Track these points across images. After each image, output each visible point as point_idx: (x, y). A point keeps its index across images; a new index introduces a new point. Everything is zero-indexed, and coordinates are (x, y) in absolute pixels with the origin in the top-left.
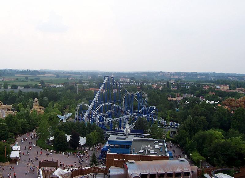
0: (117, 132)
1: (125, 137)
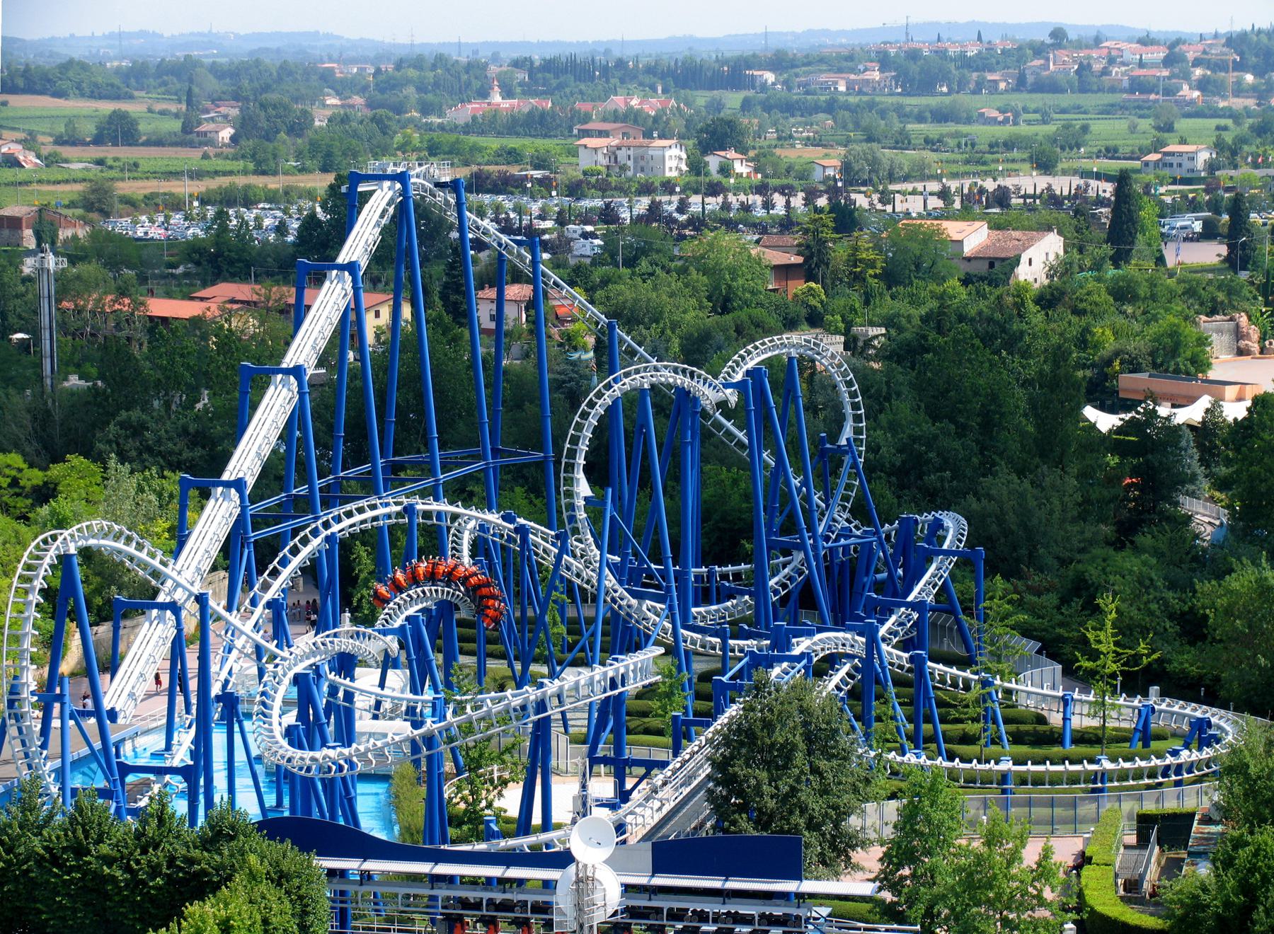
0: (495, 871)
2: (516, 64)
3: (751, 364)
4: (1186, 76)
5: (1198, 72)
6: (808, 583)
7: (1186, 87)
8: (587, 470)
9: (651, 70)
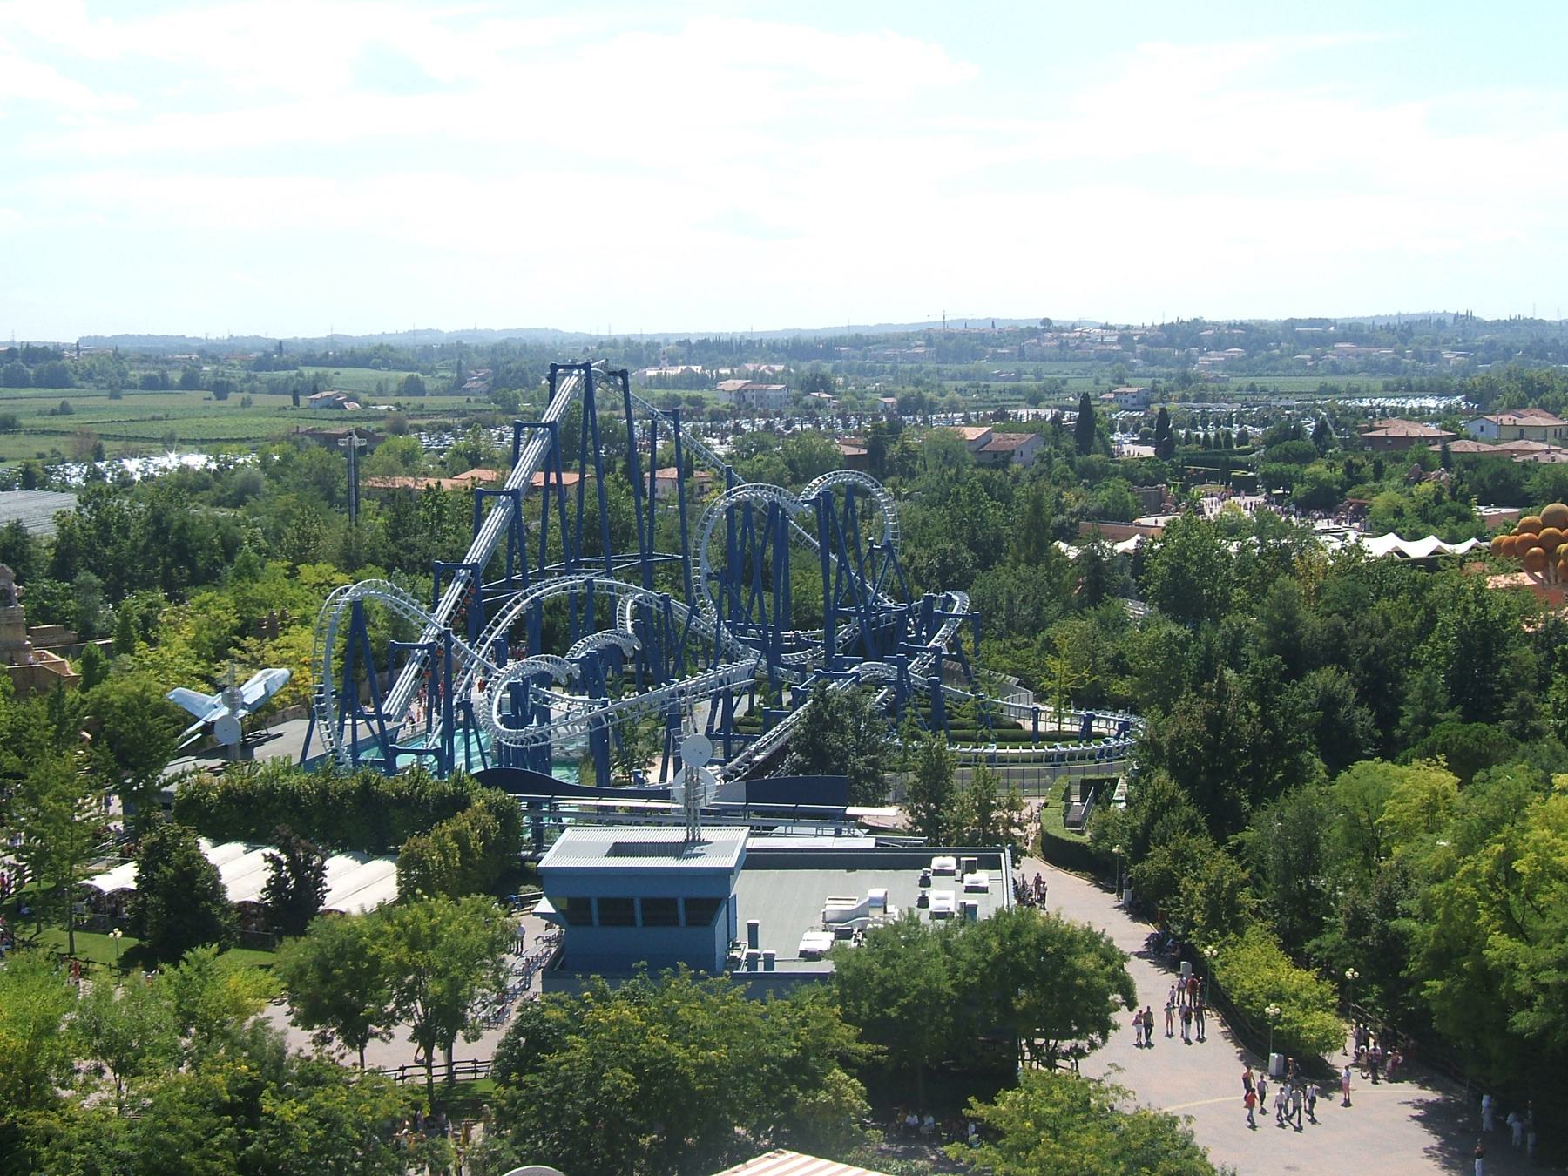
1: (677, 835)
2: (679, 343)
4: (1133, 350)
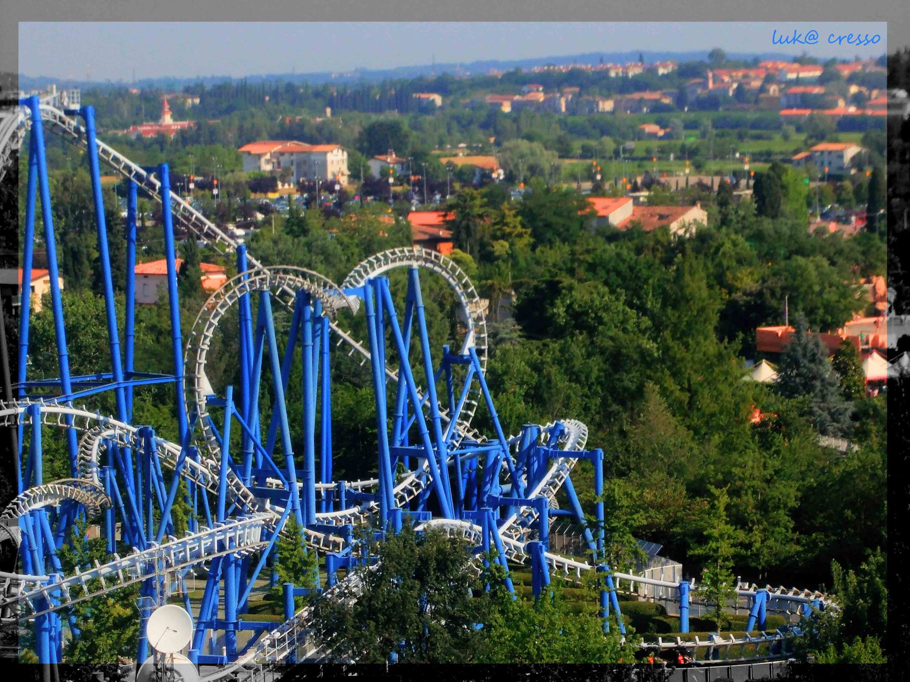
2: (189, 91)
3: (372, 275)
4: (844, 94)
5: (854, 89)
6: (432, 488)
7: (841, 103)
8: (209, 368)
9: (317, 94)
